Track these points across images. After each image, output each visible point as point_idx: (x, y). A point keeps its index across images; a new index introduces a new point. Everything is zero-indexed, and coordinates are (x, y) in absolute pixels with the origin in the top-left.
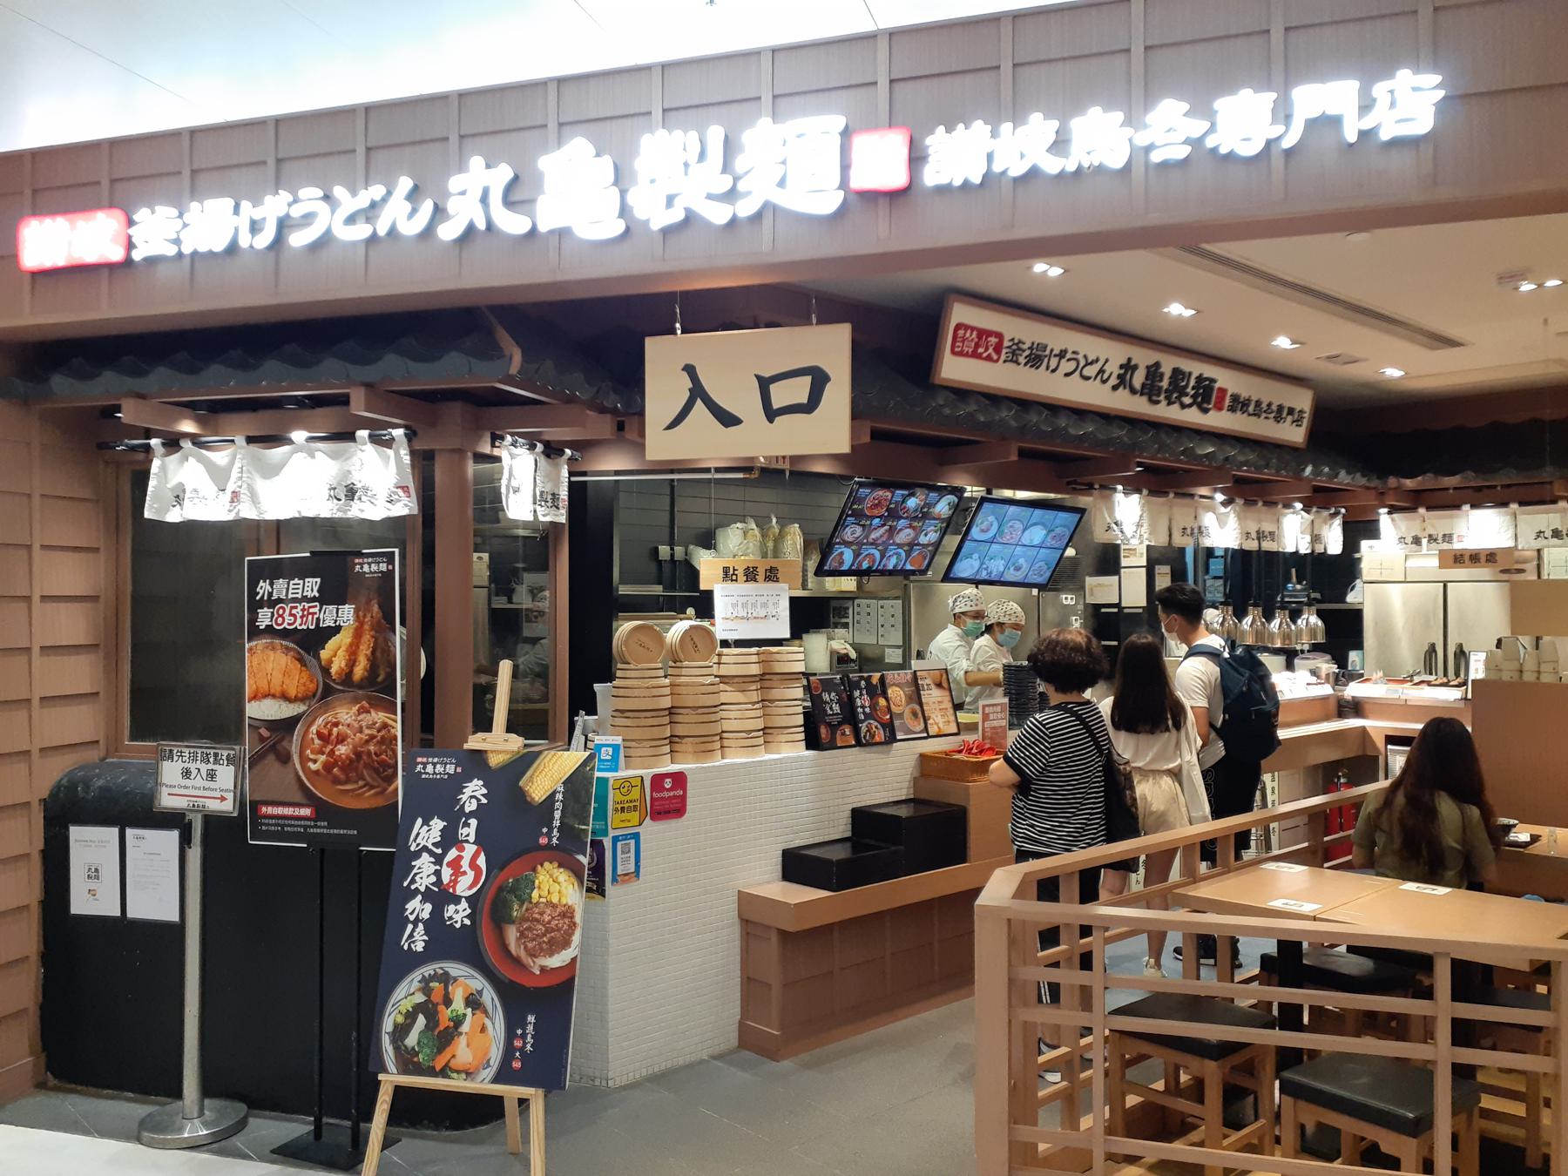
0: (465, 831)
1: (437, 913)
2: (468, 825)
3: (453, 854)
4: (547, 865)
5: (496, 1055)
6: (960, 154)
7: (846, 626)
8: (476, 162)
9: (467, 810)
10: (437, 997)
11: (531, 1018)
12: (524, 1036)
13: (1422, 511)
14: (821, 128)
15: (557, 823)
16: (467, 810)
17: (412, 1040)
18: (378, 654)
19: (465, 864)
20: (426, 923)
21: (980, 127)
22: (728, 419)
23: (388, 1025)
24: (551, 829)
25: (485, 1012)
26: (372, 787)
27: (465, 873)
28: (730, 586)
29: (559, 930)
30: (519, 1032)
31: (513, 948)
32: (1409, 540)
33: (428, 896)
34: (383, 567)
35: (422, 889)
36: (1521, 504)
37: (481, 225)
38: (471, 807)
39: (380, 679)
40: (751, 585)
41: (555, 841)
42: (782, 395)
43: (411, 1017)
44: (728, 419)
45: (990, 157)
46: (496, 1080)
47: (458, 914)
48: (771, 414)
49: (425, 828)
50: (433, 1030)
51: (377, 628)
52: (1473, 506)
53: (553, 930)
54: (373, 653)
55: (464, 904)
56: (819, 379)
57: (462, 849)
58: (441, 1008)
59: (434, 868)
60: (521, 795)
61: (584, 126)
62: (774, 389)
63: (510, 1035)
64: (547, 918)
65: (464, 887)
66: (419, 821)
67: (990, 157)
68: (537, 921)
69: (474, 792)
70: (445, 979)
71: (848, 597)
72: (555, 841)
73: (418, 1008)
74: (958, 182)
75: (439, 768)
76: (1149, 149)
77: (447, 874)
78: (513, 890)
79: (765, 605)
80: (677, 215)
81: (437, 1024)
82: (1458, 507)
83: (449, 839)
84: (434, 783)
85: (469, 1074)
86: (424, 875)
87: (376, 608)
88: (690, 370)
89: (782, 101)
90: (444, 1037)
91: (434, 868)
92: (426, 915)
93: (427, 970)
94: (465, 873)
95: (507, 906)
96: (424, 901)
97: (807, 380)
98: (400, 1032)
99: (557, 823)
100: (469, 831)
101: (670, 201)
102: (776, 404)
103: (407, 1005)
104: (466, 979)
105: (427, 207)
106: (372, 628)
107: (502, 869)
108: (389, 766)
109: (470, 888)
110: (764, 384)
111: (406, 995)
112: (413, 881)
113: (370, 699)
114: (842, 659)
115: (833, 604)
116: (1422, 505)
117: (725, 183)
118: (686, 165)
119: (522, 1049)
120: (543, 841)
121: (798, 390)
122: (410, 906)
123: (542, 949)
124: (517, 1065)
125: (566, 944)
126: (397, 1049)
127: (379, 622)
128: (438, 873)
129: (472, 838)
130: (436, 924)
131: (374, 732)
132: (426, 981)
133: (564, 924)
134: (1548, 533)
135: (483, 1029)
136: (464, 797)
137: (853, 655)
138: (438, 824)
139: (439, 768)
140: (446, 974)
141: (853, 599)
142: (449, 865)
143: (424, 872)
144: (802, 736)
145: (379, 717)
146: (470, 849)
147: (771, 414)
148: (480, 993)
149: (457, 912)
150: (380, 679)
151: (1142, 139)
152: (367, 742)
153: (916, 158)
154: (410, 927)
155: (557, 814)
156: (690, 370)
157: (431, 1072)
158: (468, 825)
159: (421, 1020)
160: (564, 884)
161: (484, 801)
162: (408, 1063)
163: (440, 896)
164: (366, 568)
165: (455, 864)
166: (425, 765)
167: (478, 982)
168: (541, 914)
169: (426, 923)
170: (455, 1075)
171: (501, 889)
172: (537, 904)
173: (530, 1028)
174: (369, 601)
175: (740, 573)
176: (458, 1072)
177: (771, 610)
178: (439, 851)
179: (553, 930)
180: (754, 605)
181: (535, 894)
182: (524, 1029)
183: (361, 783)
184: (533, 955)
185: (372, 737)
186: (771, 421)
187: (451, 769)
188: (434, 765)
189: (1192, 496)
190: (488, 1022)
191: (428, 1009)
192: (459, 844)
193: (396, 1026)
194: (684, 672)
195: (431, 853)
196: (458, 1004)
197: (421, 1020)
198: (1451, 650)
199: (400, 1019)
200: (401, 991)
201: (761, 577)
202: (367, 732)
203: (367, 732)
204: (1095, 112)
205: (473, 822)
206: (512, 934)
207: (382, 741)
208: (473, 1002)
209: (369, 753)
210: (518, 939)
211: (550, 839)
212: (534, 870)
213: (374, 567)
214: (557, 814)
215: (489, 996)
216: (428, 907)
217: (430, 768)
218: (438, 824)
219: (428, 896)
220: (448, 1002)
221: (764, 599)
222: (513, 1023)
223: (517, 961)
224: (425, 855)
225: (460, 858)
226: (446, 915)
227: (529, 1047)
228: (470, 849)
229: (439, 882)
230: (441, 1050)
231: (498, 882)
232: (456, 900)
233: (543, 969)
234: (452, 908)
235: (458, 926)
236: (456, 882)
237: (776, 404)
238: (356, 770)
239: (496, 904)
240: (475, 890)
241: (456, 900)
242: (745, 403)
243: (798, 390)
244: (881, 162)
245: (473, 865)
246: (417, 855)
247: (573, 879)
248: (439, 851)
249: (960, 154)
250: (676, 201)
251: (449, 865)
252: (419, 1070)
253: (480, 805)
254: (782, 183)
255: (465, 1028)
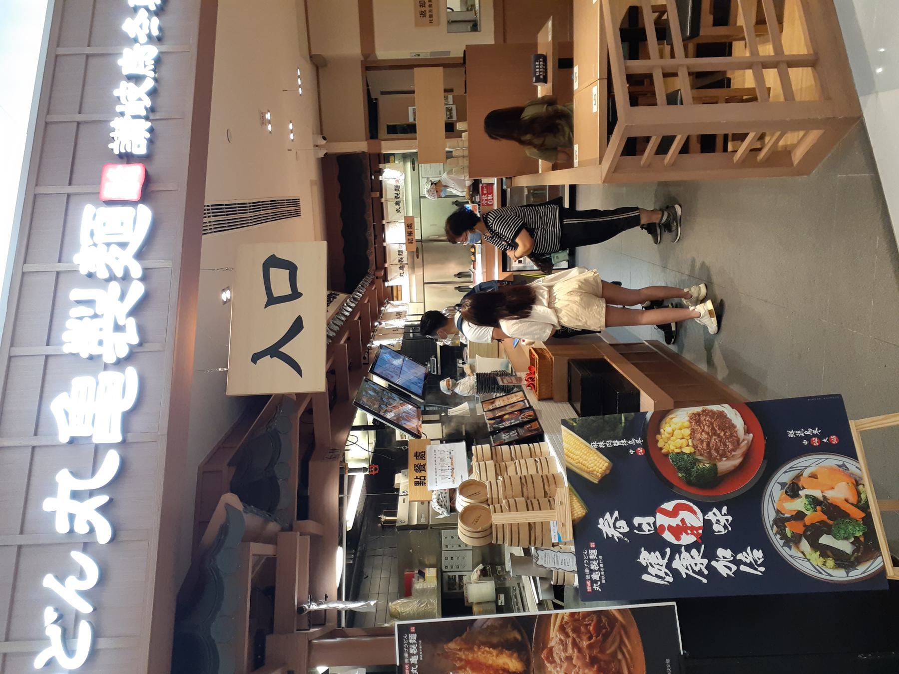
0: (646, 528)
1: (725, 541)
2: (640, 525)
3: (668, 536)
4: (660, 445)
5: (833, 460)
6: (130, 132)
7: (461, 577)
8: (48, 505)
9: (627, 529)
10: (799, 528)
11: (791, 434)
12: (808, 437)
13: (386, 265)
14: (92, 220)
15: (624, 442)
16: (627, 529)
17: (846, 547)
18: (495, 640)
19: (675, 522)
20: (735, 552)
21: (115, 123)
22: (297, 326)
23: (839, 575)
24: (630, 447)
25: (798, 477)
26: (622, 642)
27: (683, 520)
28: (429, 480)
29: (712, 424)
30: (805, 442)
31: (737, 462)
32: (401, 271)
33: (710, 555)
34: (413, 638)
35: (705, 561)
36: (383, 219)
37: (104, 499)
38: (623, 526)
39: (519, 637)
40: (428, 468)
41: (639, 441)
42: (281, 287)
43: (825, 551)
44: (297, 326)
45: (135, 117)
46: (854, 456)
47: (720, 520)
48: (295, 294)
49: (650, 569)
50: (830, 526)
51: (470, 645)
52: (384, 241)
53: (713, 429)
54: (494, 646)
55: (710, 516)
56: (273, 262)
57: (662, 526)
58: (808, 521)
59: (685, 554)
60: (606, 479)
61: (44, 399)
62: (276, 293)
63: (811, 450)
64: (704, 436)
65: (694, 519)
66: (645, 577)
67: (135, 117)
68: (708, 444)
69: (611, 526)
70: (780, 522)
71: (440, 574)
72: (639, 441)
73: (815, 545)
74: (148, 135)
75: (594, 566)
76: (150, 36)
77: (687, 539)
78: (687, 471)
79: (442, 459)
80: (131, 324)
81: (822, 522)
82: (384, 248)
83: (655, 542)
84: (608, 569)
85: (857, 483)
86: (692, 562)
87: (452, 645)
88: (256, 358)
89: (65, 242)
90: (834, 514)
91: (685, 554)
92: (728, 553)
93: (777, 542)
94: (683, 520)
95: (702, 474)
96: (715, 557)
97: (273, 271)
98: (843, 561)
99: (624, 442)
100: (644, 522)
101: (118, 328)
102: (289, 292)
103: (815, 557)
104: (775, 502)
105: (78, 557)
106: (471, 649)
107: (671, 486)
108: (599, 621)
109: (694, 513)
110: (272, 300)
111: (805, 560)
112: (700, 573)
113: (539, 650)
114: (484, 574)
115: (446, 589)
116: (383, 265)
117: (115, 287)
118: (95, 316)
119: (820, 437)
120: (641, 451)
121: (279, 277)
122: (724, 572)
123: (731, 436)
124: (834, 439)
125: (721, 415)
126: (859, 561)
127: (466, 642)
128: (688, 548)
129: (651, 519)
130: (736, 540)
131: (569, 641)
132: (788, 542)
133: (705, 420)
134: (398, 207)
135: (813, 476)
136: (616, 535)
137: (481, 566)
138: (645, 557)
139: (594, 566)
140: (776, 522)
141: (442, 572)
142: (678, 539)
143: (690, 563)
144: (536, 444)
145: (554, 635)
146: (662, 520)
147: (295, 294)
148: (783, 485)
149: (718, 522)
150: (519, 637)
151: (143, 39)
152: (580, 650)
153: (127, 158)
154: (743, 568)
155: (617, 443)
156: (256, 358)
157: (868, 520)
158: (640, 525)
159: (825, 540)
160: (673, 426)
161: (616, 514)
162: (867, 547)
163: (708, 542)
164: (414, 660)
165: (677, 531)
166: (593, 582)
167: (774, 491)
168: (702, 442)
169: (735, 552)
170: (863, 496)
171: (689, 483)
172: (694, 447)
173: (800, 433)
174: (446, 655)
175: (419, 475)
176: (859, 494)
177: (446, 455)
178: (668, 550)
179: (713, 429)
180: (442, 466)
181: (687, 450)
182: (802, 438)
183: (620, 656)
184: (737, 443)
185: (575, 644)
186: (300, 295)
187: (593, 554)
188: (592, 571)
189: (377, 356)
190: (806, 473)
191: (813, 534)
192: (658, 530)
193: (838, 566)
194: (495, 496)
195: (672, 559)
196: (799, 505)
197: (825, 540)
198: (457, 279)
199: (830, 562)
200: (805, 567)
201: (422, 462)
202: (570, 651)
203: (570, 651)
204: (120, 62)
205: (637, 521)
206: (725, 465)
207: (576, 630)
208: (793, 490)
209: (590, 647)
210: (728, 458)
211: (638, 445)
212: (666, 455)
213: (413, 650)
214: (617, 443)
215: (784, 476)
216: (721, 552)
217: (596, 576)
218: (645, 557)
219: (710, 555)
220: (800, 516)
221: (438, 460)
222: (800, 450)
223: (747, 456)
224: (676, 564)
225: (670, 528)
226: (724, 532)
227: (816, 432)
228: (662, 520)
229: (695, 545)
230: (845, 515)
231: (686, 488)
232: (708, 524)
233: (747, 431)
234: (716, 528)
235: (730, 518)
236: (692, 528)
237: (289, 292)
238: (607, 663)
239: (704, 486)
240: (695, 508)
241: (708, 524)
242: (285, 314)
243: (279, 277)
244: (125, 181)
245: (673, 514)
246: (675, 573)
247: (667, 419)
248: (668, 550)
249: (130, 132)
250: (121, 323)
251: (678, 539)
252: (870, 533)
253: (621, 517)
254: (123, 245)
255: (818, 494)
